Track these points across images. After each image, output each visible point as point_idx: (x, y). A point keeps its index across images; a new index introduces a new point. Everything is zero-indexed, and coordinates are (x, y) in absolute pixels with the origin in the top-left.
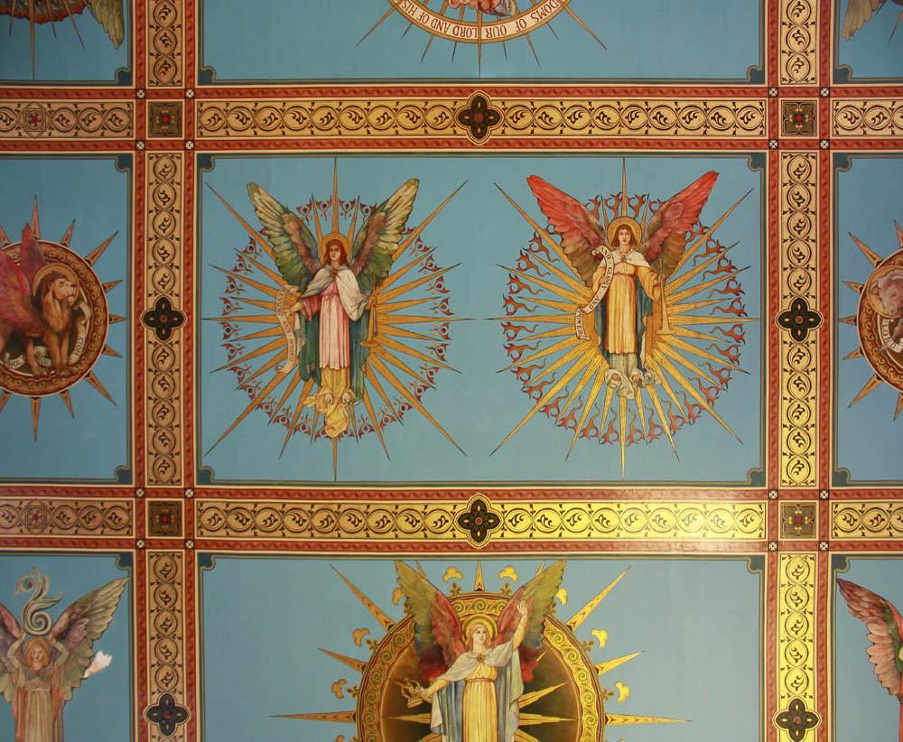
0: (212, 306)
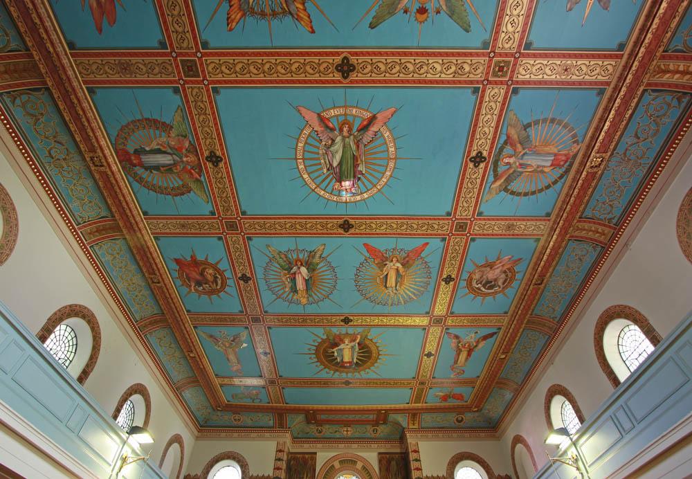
0: (260, 273)
